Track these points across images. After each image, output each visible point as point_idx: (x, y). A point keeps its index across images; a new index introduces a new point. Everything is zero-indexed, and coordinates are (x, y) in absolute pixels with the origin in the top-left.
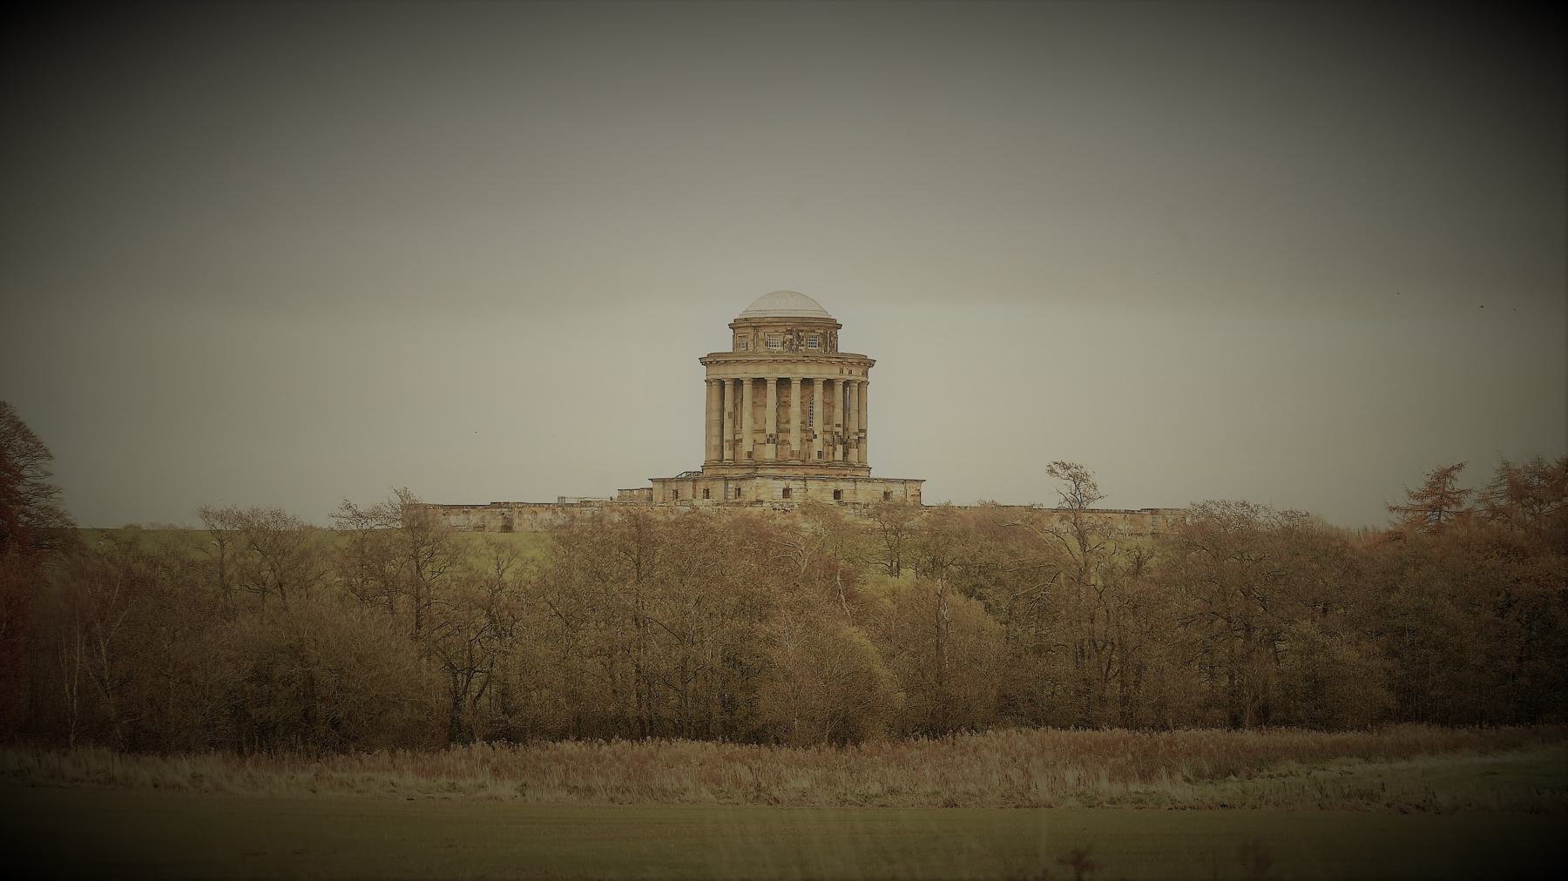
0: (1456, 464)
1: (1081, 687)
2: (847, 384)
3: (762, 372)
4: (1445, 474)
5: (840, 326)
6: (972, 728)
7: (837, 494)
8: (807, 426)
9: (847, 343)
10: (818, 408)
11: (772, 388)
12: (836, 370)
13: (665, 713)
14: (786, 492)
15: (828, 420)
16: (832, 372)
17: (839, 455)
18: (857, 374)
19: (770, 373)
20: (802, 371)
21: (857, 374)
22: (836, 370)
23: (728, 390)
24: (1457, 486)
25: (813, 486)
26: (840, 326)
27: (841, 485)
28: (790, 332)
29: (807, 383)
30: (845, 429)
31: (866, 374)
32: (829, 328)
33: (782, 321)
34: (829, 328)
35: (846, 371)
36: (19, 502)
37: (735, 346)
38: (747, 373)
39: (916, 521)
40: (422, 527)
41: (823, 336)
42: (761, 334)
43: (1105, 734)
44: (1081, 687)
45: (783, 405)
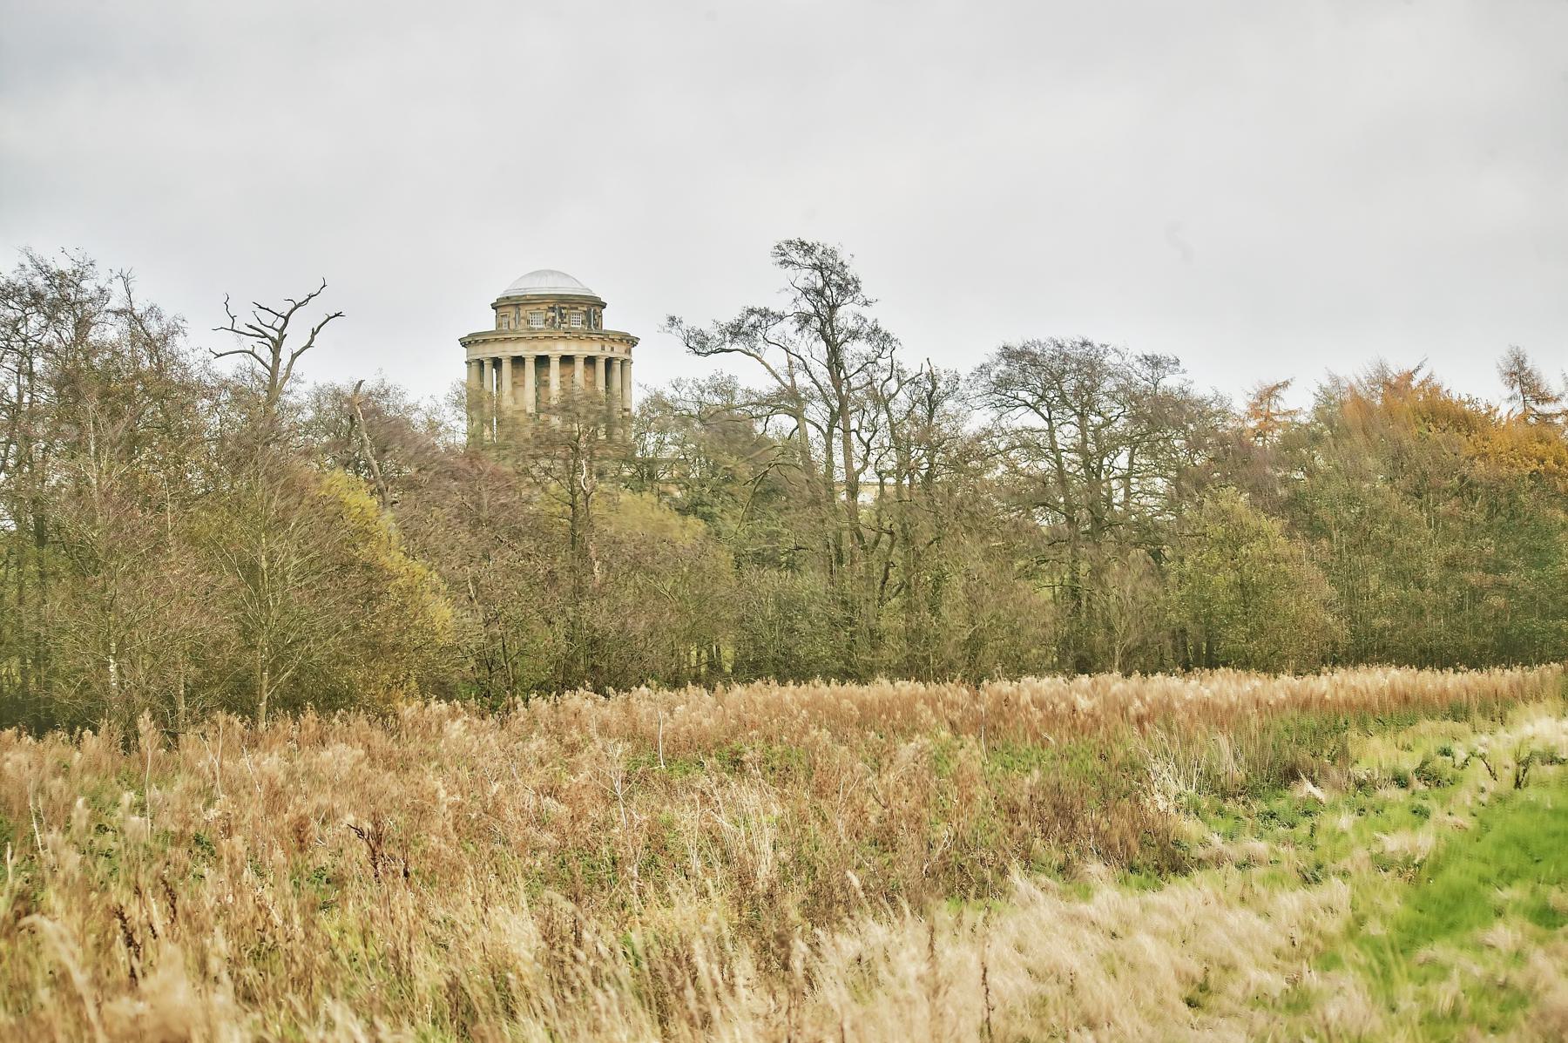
0: (1280, 381)
1: (838, 614)
2: (609, 362)
3: (520, 350)
4: (1270, 393)
5: (603, 306)
6: (1034, 673)
9: (611, 321)
11: (530, 366)
16: (593, 349)
18: (619, 351)
19: (528, 351)
20: (562, 348)
21: (619, 351)
24: (1284, 406)
26: (603, 306)
28: (553, 309)
29: (567, 360)
30: (610, 409)
31: (628, 352)
32: (593, 306)
33: (542, 299)
34: (593, 306)
35: (608, 348)
37: (499, 325)
38: (506, 351)
41: (587, 313)
42: (522, 313)
43: (882, 688)
44: (838, 614)
45: (542, 384)
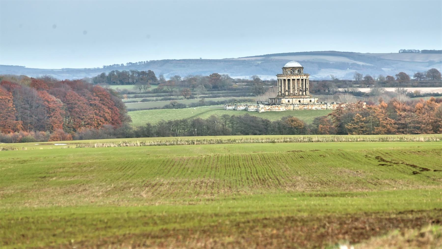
7: (299, 101)
8: (294, 88)
10: (296, 85)
12: (299, 77)
13: (62, 197)
14: (289, 101)
15: (298, 86)
17: (301, 93)
20: (293, 78)
22: (299, 77)
23: (283, 81)
25: (294, 100)
27: (300, 99)
36: (206, 237)
39: (131, 131)
40: (268, 124)
45: (285, 84)
